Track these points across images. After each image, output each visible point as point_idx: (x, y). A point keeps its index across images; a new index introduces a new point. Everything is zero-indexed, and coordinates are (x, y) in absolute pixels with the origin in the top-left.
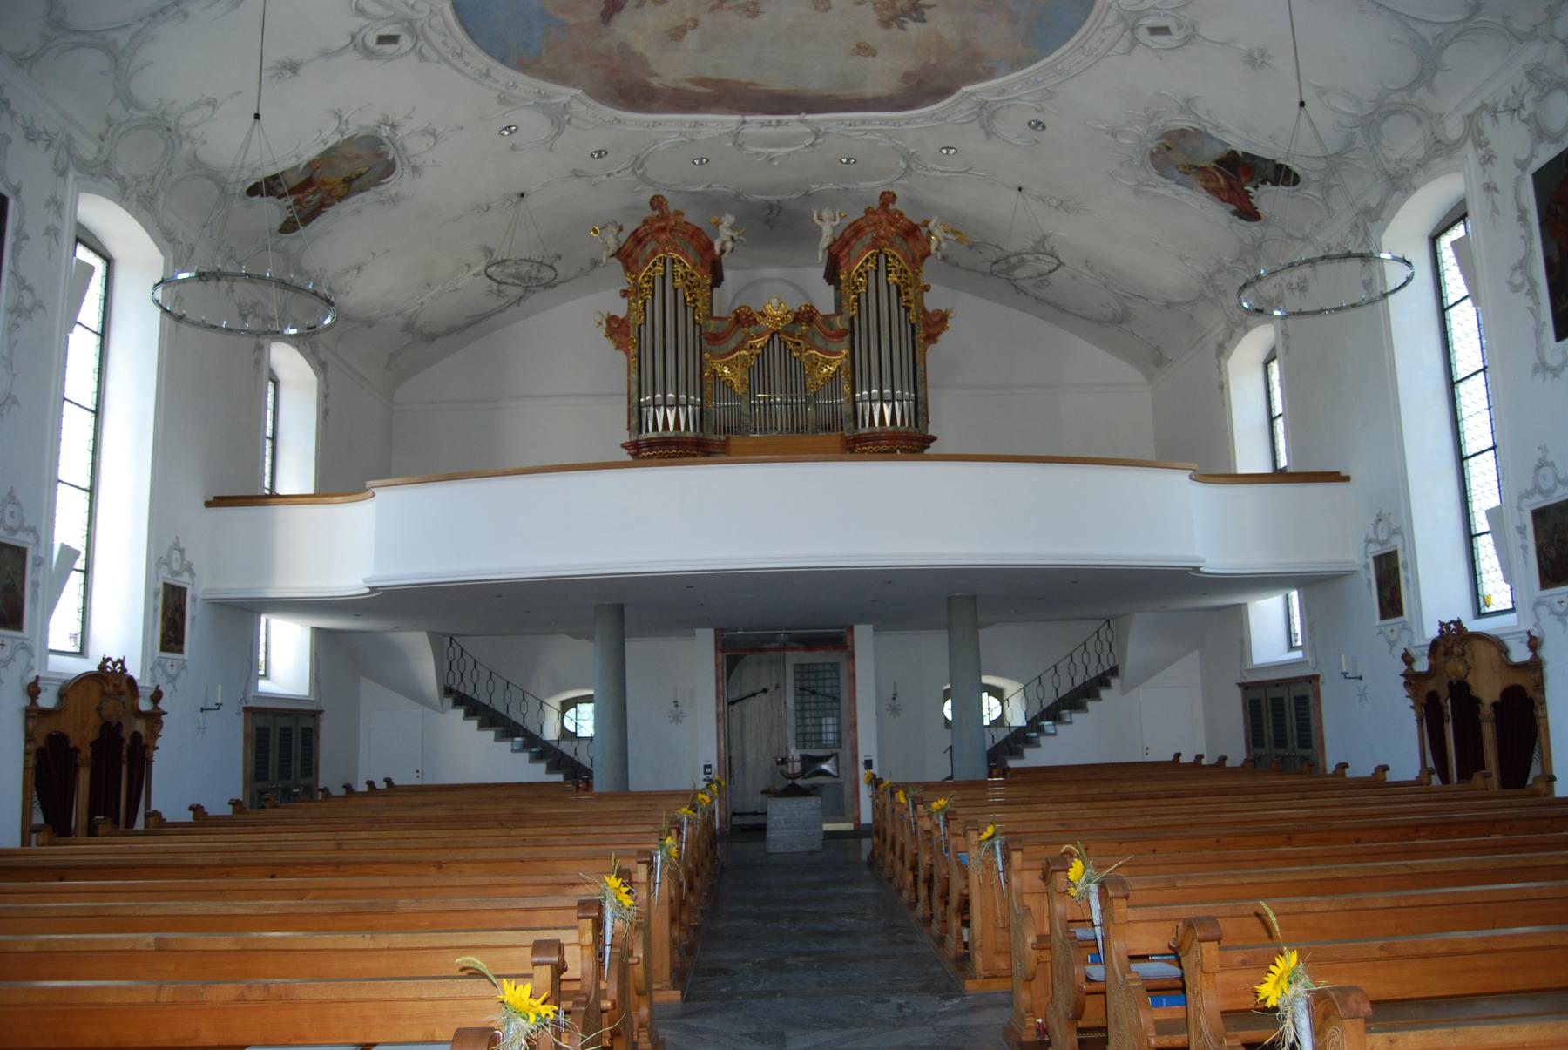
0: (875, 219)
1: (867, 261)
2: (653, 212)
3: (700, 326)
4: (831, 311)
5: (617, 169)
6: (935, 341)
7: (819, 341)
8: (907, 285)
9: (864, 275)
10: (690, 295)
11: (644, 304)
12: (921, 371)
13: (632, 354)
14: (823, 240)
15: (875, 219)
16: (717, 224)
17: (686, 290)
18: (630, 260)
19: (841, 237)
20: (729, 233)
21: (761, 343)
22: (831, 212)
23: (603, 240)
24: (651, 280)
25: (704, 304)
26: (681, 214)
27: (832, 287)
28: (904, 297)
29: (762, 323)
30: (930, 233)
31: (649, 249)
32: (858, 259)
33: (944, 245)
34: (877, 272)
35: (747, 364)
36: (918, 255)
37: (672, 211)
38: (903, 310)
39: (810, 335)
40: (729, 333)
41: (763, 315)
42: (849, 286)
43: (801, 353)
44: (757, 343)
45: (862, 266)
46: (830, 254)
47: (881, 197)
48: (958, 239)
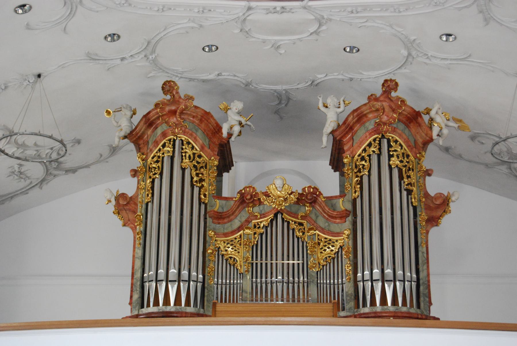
0: (378, 105)
1: (370, 145)
2: (165, 97)
3: (206, 205)
7: (321, 222)
8: (409, 169)
9: (367, 158)
10: (197, 175)
11: (153, 182)
12: (423, 253)
13: (138, 230)
15: (378, 105)
16: (226, 109)
18: (141, 142)
19: (344, 123)
21: (264, 223)
22: (336, 100)
23: (118, 123)
24: (160, 160)
26: (192, 98)
27: (338, 173)
30: (432, 120)
31: (159, 131)
32: (361, 143)
33: (445, 131)
34: (379, 156)
35: (251, 242)
36: (420, 141)
38: (405, 193)
39: (313, 216)
41: (267, 195)
43: (304, 233)
44: (261, 222)
45: (365, 150)
47: (383, 85)
48: (459, 126)
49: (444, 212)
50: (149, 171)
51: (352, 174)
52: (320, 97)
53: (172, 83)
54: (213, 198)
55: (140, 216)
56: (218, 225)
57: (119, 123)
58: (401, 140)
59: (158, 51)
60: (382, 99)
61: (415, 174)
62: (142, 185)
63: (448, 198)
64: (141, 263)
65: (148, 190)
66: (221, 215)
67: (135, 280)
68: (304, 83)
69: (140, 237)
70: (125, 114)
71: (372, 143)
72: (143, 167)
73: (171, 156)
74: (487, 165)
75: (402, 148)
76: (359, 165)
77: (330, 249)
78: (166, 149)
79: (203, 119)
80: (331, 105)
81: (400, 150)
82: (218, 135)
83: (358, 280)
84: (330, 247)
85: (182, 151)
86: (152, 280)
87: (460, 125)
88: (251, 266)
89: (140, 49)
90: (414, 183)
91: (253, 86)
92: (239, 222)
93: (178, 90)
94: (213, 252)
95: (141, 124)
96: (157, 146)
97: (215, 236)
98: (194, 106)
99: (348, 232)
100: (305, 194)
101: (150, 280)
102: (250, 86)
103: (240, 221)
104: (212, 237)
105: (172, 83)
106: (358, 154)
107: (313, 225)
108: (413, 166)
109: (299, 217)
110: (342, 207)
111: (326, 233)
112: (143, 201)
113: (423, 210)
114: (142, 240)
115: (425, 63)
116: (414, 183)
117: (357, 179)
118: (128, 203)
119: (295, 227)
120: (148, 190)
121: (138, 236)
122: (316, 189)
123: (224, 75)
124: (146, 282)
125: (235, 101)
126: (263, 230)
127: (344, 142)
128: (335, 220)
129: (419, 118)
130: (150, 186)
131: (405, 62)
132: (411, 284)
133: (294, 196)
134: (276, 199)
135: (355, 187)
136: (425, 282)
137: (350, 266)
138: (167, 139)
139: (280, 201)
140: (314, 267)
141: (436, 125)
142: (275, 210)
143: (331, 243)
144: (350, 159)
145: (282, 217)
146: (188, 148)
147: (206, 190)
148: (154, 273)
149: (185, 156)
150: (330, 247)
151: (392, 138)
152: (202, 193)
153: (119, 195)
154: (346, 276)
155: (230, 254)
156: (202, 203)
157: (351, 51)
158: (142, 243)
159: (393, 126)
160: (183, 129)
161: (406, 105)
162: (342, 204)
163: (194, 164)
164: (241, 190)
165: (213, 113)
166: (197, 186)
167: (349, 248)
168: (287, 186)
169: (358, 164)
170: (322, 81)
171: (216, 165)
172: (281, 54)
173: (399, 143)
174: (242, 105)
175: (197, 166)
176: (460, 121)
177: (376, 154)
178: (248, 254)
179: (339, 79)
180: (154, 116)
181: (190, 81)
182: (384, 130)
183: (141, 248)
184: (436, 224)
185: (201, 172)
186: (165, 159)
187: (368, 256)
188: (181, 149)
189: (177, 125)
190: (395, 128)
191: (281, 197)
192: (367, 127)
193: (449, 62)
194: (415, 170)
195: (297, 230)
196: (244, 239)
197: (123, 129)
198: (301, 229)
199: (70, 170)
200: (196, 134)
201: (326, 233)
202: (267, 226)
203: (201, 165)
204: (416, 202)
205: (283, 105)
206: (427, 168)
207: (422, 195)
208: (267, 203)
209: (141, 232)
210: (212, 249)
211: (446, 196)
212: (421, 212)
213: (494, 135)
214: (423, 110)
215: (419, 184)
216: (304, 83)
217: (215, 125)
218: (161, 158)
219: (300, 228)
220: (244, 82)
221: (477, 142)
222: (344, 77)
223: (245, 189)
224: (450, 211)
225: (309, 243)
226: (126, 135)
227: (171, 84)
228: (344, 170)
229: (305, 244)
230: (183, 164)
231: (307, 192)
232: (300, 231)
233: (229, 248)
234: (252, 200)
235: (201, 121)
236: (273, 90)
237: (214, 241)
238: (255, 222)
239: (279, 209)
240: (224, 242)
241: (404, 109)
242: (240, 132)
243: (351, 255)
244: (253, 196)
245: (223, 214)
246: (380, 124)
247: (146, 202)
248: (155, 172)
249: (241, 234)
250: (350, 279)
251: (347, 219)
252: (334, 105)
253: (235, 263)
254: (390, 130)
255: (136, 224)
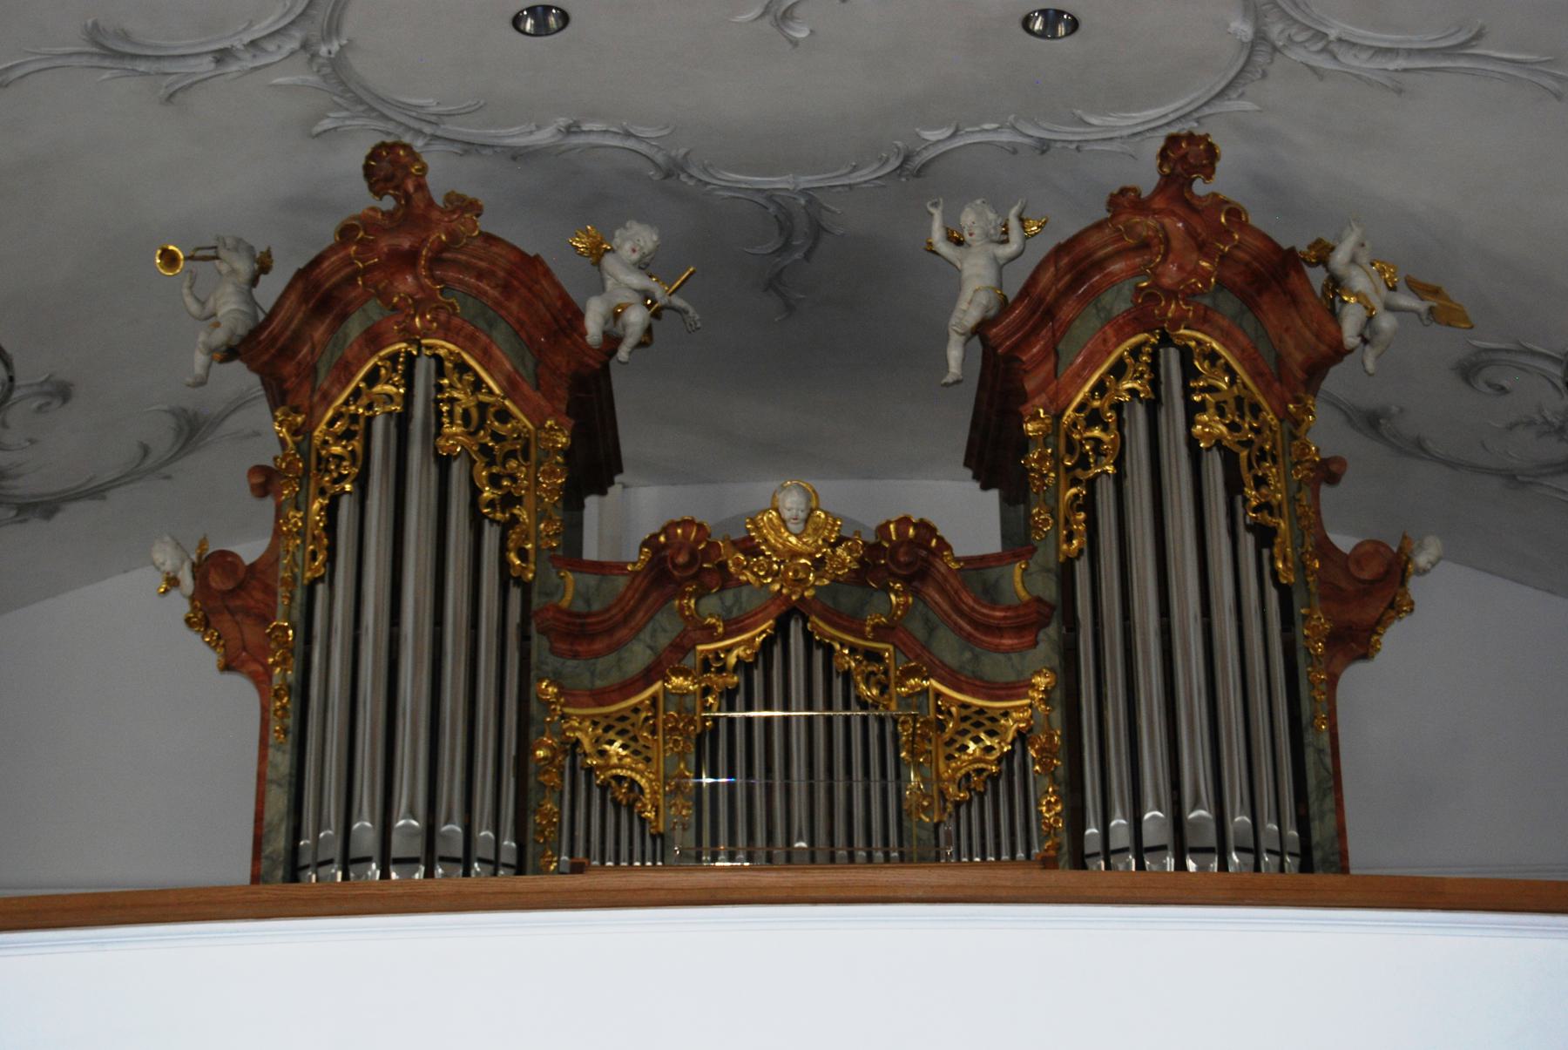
0: (1146, 225)
1: (1119, 370)
2: (373, 201)
3: (526, 588)
4: (992, 544)
5: (247, 39)
6: (1366, 652)
7: (947, 647)
8: (1263, 455)
9: (1110, 415)
10: (494, 481)
11: (331, 511)
12: (1320, 751)
13: (277, 682)
14: (963, 305)
15: (1146, 225)
16: (597, 254)
17: (479, 464)
18: (288, 369)
19: (1025, 292)
20: (637, 280)
21: (739, 651)
22: (991, 216)
23: (202, 303)
24: (354, 430)
25: (541, 516)
26: (474, 207)
27: (993, 495)
28: (1250, 492)
29: (747, 576)
30: (1336, 283)
31: (355, 328)
32: (1090, 364)
33: (1386, 322)
34: (1153, 406)
35: (691, 722)
36: (1297, 357)
37: (439, 201)
38: (1248, 542)
39: (917, 628)
40: (628, 616)
41: (749, 548)
42: (1057, 459)
43: (884, 689)
44: (728, 650)
45: (1100, 387)
46: (989, 354)
47: (1163, 155)
48: (1431, 310)
49: (1391, 606)
50: (319, 470)
51: (1057, 475)
52: (935, 205)
53: (402, 153)
54: (550, 565)
55: (285, 629)
56: (571, 663)
57: (210, 304)
58: (1231, 352)
59: (349, 28)
60: (1158, 204)
61: (1282, 475)
62: (293, 521)
63: (1404, 558)
64: (289, 800)
65: (314, 537)
66: (582, 625)
67: (265, 864)
68: (876, 166)
69: (283, 707)
70: (233, 271)
71: (1128, 361)
72: (294, 455)
73: (399, 415)
74: (1512, 478)
75: (1232, 382)
76: (1080, 442)
77: (981, 745)
78: (378, 388)
79: (515, 283)
80: (977, 231)
81: (1225, 387)
82: (568, 342)
83: (1088, 850)
84: (983, 736)
85: (439, 396)
86: (328, 857)
87: (1435, 304)
88: (694, 808)
89: (284, 15)
90: (1280, 505)
91: (691, 177)
92: (649, 652)
93: (423, 176)
94: (554, 758)
95: (288, 303)
96: (348, 382)
97: (562, 700)
98: (480, 233)
99: (1048, 680)
100: (887, 545)
101: (321, 859)
102: (683, 177)
103: (651, 648)
104: (549, 703)
105: (402, 153)
106: (1075, 404)
107: (917, 657)
108: (1274, 447)
109: (868, 629)
110: (1023, 594)
111: (965, 686)
112: (294, 578)
113: (1316, 602)
114: (291, 715)
115: (1313, 69)
116: (1280, 505)
117: (1074, 490)
118: (241, 587)
119: (853, 664)
120: (314, 537)
121: (278, 704)
122: (925, 528)
123: (590, 132)
124: (307, 867)
125: (628, 224)
126: (736, 679)
127: (1024, 363)
128: (997, 641)
129: (1293, 273)
130: (321, 524)
131: (1242, 70)
132: (1282, 861)
133: (850, 551)
134: (783, 562)
135: (1067, 522)
136: (1332, 858)
137: (1056, 801)
138: (382, 353)
139: (799, 567)
140: (925, 810)
141: (1352, 300)
142: (778, 602)
143: (986, 722)
144: (1047, 421)
145: (805, 629)
146: (459, 386)
147: (527, 536)
148: (336, 833)
149: (451, 413)
150: (983, 736)
151: (1199, 342)
152: (511, 545)
153: (207, 559)
154: (1044, 838)
155: (615, 767)
156: (512, 582)
157: (1049, 32)
158: (291, 729)
159: (1199, 304)
160: (443, 317)
161: (1244, 226)
162: (1023, 583)
163: (483, 441)
164: (655, 537)
165: (550, 260)
166: (493, 521)
167: (1052, 736)
168: (823, 516)
169: (1077, 437)
170: (937, 156)
171: (561, 449)
172: (795, 43)
173: (1222, 361)
174: (655, 238)
175: (492, 449)
176: (1436, 292)
177: (1141, 400)
178: (682, 766)
179: (1000, 146)
180: (338, 271)
181: (466, 152)
182: (1170, 315)
183: (288, 747)
184: (1362, 651)
185: (509, 471)
186: (378, 426)
187: (1125, 774)
188: (433, 391)
189: (419, 307)
190: (1206, 308)
191: (801, 555)
192: (1108, 307)
193: (1401, 63)
194: (1280, 460)
195: (859, 678)
196: (665, 711)
197: (222, 325)
198: (873, 673)
199: (35, 505)
200: (489, 336)
201: (965, 686)
202: (751, 663)
203: (508, 447)
204: (1289, 569)
205: (798, 255)
206: (1325, 454)
207: (1310, 549)
208: (751, 578)
209: (289, 687)
210: (550, 747)
211: (1395, 549)
212: (1309, 606)
213: (1548, 357)
214: (1305, 249)
215: (1299, 511)
216: (876, 166)
217: (559, 304)
218: (362, 421)
219: (870, 669)
220: (660, 158)
221: (1481, 385)
222: (1020, 139)
223: (670, 531)
224: (1412, 603)
225: (904, 722)
226: (235, 341)
227: (398, 154)
228: (1026, 459)
229: (889, 728)
230: (441, 442)
231: (894, 538)
232: (873, 679)
233: (611, 743)
234: (695, 569)
235: (506, 289)
236: (765, 190)
237: (556, 718)
238: (708, 651)
239: (794, 598)
240: (595, 724)
241: (1240, 242)
242: (649, 331)
243: (1059, 763)
244: (700, 557)
245: (589, 620)
246: (1156, 295)
247: (306, 582)
248: (340, 474)
249: (656, 693)
250: (1058, 847)
251: (1041, 635)
252: (987, 235)
253: (637, 799)
254: (1191, 314)
255: (271, 660)
